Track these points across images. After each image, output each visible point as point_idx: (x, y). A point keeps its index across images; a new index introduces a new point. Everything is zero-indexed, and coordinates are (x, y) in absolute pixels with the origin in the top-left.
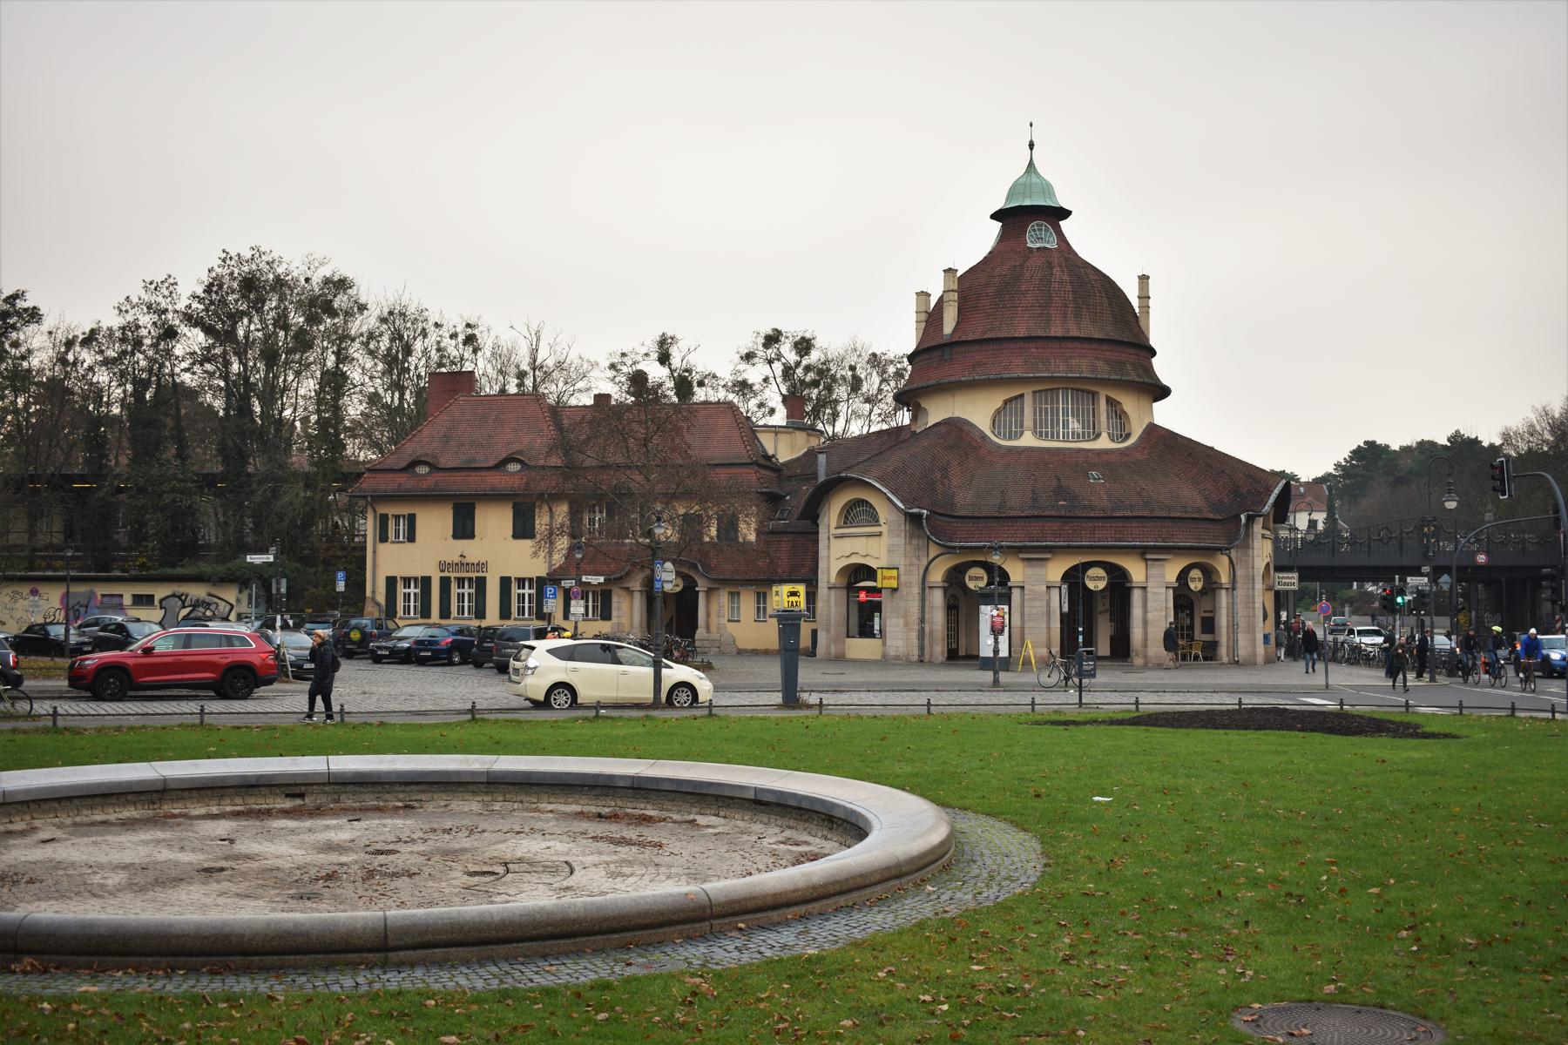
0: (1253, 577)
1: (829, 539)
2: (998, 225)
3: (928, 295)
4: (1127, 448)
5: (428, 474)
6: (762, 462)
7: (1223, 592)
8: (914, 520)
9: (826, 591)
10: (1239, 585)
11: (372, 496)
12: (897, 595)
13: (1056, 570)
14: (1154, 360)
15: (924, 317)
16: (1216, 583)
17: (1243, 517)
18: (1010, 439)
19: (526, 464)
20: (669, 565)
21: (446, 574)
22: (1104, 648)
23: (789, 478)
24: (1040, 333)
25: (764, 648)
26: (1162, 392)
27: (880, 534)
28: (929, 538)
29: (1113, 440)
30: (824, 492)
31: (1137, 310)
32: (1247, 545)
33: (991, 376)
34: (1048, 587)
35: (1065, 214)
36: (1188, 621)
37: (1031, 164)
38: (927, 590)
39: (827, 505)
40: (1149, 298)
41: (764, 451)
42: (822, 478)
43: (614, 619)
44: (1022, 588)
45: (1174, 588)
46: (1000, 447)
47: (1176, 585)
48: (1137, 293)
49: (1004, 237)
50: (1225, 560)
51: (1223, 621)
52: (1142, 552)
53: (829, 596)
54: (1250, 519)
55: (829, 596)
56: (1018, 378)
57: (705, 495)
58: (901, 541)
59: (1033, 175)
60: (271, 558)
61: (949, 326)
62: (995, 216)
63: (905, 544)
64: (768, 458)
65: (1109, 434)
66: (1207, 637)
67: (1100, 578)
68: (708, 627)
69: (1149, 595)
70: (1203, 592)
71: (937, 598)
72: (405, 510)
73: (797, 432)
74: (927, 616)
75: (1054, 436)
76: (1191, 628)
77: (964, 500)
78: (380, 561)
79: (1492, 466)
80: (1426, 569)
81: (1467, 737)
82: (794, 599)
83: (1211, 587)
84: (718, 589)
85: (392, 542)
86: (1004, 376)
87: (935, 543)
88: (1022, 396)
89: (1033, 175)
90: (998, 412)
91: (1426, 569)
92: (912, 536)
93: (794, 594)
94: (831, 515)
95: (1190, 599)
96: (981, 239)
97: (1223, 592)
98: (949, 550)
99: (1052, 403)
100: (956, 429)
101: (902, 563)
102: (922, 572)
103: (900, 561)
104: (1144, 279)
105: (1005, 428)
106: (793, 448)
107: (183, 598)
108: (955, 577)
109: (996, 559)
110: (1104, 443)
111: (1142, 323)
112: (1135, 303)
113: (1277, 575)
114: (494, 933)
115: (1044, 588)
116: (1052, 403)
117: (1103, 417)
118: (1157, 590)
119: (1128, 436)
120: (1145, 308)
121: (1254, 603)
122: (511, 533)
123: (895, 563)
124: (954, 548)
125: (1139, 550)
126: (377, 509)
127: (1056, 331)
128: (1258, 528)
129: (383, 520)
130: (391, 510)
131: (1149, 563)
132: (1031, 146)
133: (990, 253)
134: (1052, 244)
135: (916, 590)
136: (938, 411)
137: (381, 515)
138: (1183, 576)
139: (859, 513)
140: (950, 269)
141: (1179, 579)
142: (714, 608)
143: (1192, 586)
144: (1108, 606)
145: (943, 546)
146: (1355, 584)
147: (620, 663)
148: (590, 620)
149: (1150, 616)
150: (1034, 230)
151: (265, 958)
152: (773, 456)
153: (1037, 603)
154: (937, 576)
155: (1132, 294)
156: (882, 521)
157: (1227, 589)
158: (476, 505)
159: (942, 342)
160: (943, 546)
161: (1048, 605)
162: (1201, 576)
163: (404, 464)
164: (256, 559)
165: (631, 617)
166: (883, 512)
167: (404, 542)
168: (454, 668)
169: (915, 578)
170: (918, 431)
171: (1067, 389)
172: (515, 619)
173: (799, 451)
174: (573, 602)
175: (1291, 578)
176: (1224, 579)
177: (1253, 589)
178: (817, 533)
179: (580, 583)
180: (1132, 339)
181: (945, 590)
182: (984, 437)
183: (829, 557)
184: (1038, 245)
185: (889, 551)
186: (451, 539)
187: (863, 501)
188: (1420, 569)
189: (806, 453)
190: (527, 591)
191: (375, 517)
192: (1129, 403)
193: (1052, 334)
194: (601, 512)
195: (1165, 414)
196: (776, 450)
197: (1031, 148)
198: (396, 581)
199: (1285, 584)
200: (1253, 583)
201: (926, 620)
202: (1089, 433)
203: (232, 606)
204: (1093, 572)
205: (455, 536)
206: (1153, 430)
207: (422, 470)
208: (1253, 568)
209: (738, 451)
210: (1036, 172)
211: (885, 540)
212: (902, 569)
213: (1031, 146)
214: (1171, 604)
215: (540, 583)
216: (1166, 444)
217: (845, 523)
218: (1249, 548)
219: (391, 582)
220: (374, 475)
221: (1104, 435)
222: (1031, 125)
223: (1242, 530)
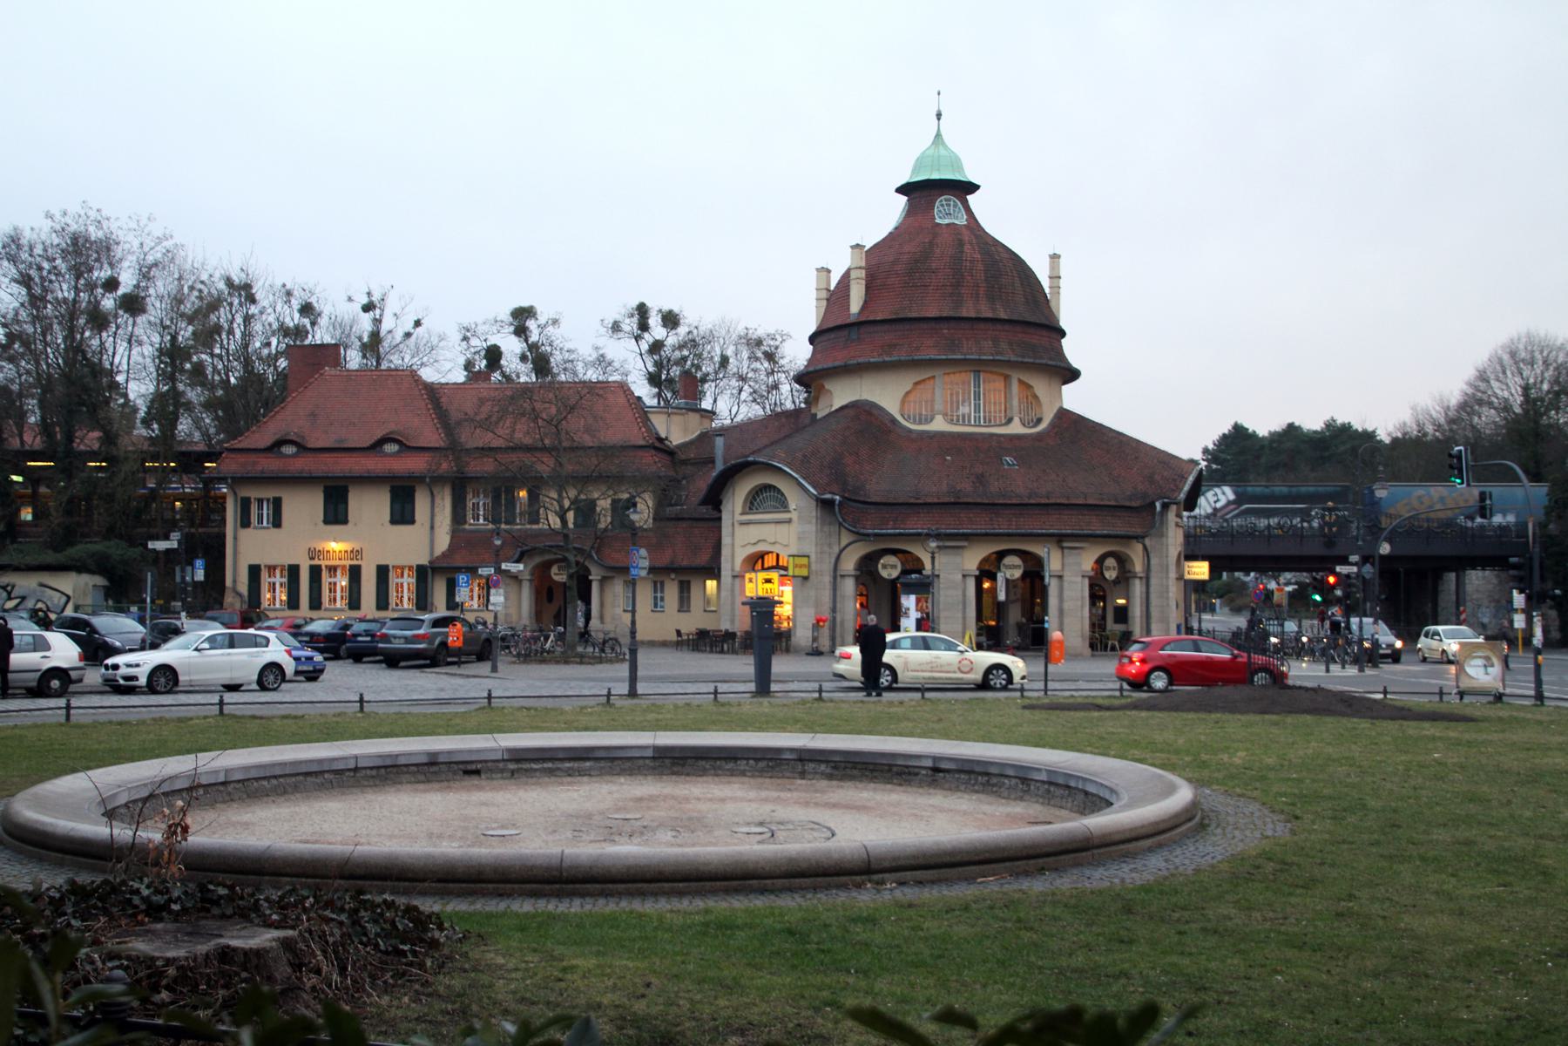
0: (1167, 566)
1: (733, 525)
2: (903, 199)
3: (829, 271)
4: (1038, 434)
5: (294, 456)
6: (657, 444)
7: (1137, 582)
8: (825, 505)
9: (729, 579)
11: (232, 478)
12: (809, 584)
13: (1086, 560)
14: (1063, 341)
15: (824, 294)
16: (1130, 572)
18: (920, 423)
19: (405, 445)
20: (643, 552)
21: (316, 562)
22: (784, 648)
23: (684, 462)
24: (952, 314)
25: (661, 639)
26: (1072, 375)
27: (789, 521)
28: (840, 524)
29: (1024, 425)
30: (733, 473)
31: (1047, 290)
32: (1162, 535)
33: (903, 358)
34: (964, 576)
35: (972, 188)
37: (938, 135)
38: (839, 578)
39: (731, 490)
40: (1060, 277)
41: (657, 434)
42: (720, 466)
45: (1090, 578)
46: (910, 431)
47: (977, 573)
48: (1047, 273)
49: (911, 211)
50: (1139, 547)
51: (1137, 612)
52: (1059, 539)
53: (733, 585)
54: (1165, 506)
55: (733, 585)
56: (930, 360)
57: (613, 480)
58: (812, 528)
59: (941, 147)
60: (175, 545)
61: (855, 305)
62: (901, 190)
63: (817, 532)
64: (661, 440)
66: (1120, 628)
67: (1015, 567)
68: (602, 618)
69: (1066, 585)
70: (1116, 582)
71: (849, 586)
72: (270, 493)
73: (690, 413)
74: (838, 605)
77: (878, 486)
78: (242, 548)
79: (1450, 456)
80: (1354, 558)
82: (768, 586)
83: (1125, 577)
84: (613, 578)
85: (255, 528)
86: (916, 358)
87: (846, 528)
88: (934, 377)
89: (941, 147)
90: (908, 393)
91: (1354, 558)
92: (823, 524)
93: (768, 581)
94: (736, 497)
96: (889, 213)
97: (1137, 582)
98: (862, 537)
100: (863, 413)
101: (813, 549)
102: (833, 560)
103: (810, 549)
104: (1055, 257)
106: (686, 430)
107: (9, 588)
108: (867, 569)
109: (1039, 550)
110: (1016, 428)
111: (1053, 305)
114: (948, 858)
117: (1015, 402)
118: (1073, 579)
119: (1039, 421)
120: (1056, 288)
121: (1168, 592)
122: (388, 517)
123: (806, 551)
124: (868, 535)
125: (1055, 539)
126: (238, 491)
127: (968, 311)
128: (1171, 516)
129: (245, 505)
130: (253, 493)
131: (1066, 551)
132: (939, 116)
133: (896, 228)
134: (961, 220)
135: (827, 579)
136: (841, 394)
137: (242, 499)
139: (765, 499)
140: (858, 245)
142: (609, 598)
145: (857, 533)
146: (1225, 574)
149: (1066, 606)
150: (942, 205)
151: (775, 881)
152: (667, 439)
154: (849, 564)
156: (792, 506)
157: (1141, 578)
158: (417, 488)
159: (848, 321)
160: (857, 533)
161: (964, 595)
162: (1116, 565)
163: (269, 443)
164: (160, 545)
165: (520, 607)
166: (794, 499)
167: (268, 528)
168: (341, 662)
169: (827, 566)
170: (819, 416)
171: (979, 371)
172: (393, 610)
173: (693, 433)
176: (1138, 567)
178: (720, 519)
179: (499, 570)
180: (1043, 321)
181: (857, 578)
182: (894, 421)
183: (733, 545)
184: (946, 221)
185: (799, 538)
186: (388, 524)
187: (775, 487)
188: (1347, 558)
189: (699, 435)
191: (236, 501)
192: (1040, 386)
193: (965, 314)
194: (219, 489)
195: (1074, 398)
196: (668, 432)
197: (939, 119)
198: (321, 570)
200: (1167, 572)
201: (838, 609)
202: (1000, 417)
203: (69, 598)
204: (1009, 560)
205: (394, 521)
206: (1064, 416)
207: (289, 450)
208: (1167, 557)
209: (637, 437)
210: (943, 143)
211: (795, 528)
213: (939, 116)
216: (1071, 424)
217: (750, 509)
219: (255, 571)
220: (233, 456)
221: (1016, 420)
222: (939, 94)
223: (1157, 518)
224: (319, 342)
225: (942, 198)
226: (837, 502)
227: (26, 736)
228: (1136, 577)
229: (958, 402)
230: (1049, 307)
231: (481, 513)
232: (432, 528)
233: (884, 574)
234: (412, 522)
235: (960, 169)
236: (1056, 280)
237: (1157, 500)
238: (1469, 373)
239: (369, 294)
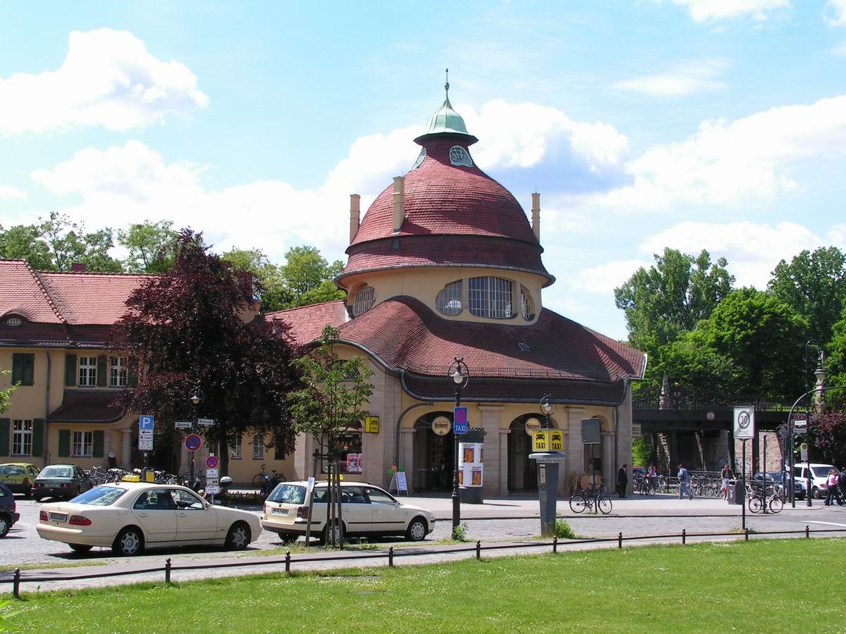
16: (604, 431)
25: (239, 482)
26: (550, 280)
31: (530, 220)
35: (473, 140)
65: (470, 311)
75: (483, 315)
81: (111, 429)
111: (535, 231)
132: (447, 86)
147: (414, 541)
148: (82, 457)
150: (454, 152)
154: (410, 422)
190: (23, 432)
195: (551, 299)
197: (447, 90)
212: (382, 417)
213: (447, 86)
215: (39, 425)
222: (447, 71)
227: (731, 501)
229: (505, 303)
231: (118, 377)
232: (48, 388)
233: (437, 431)
234: (31, 383)
235: (464, 128)
238: (250, 249)
239: (656, 256)
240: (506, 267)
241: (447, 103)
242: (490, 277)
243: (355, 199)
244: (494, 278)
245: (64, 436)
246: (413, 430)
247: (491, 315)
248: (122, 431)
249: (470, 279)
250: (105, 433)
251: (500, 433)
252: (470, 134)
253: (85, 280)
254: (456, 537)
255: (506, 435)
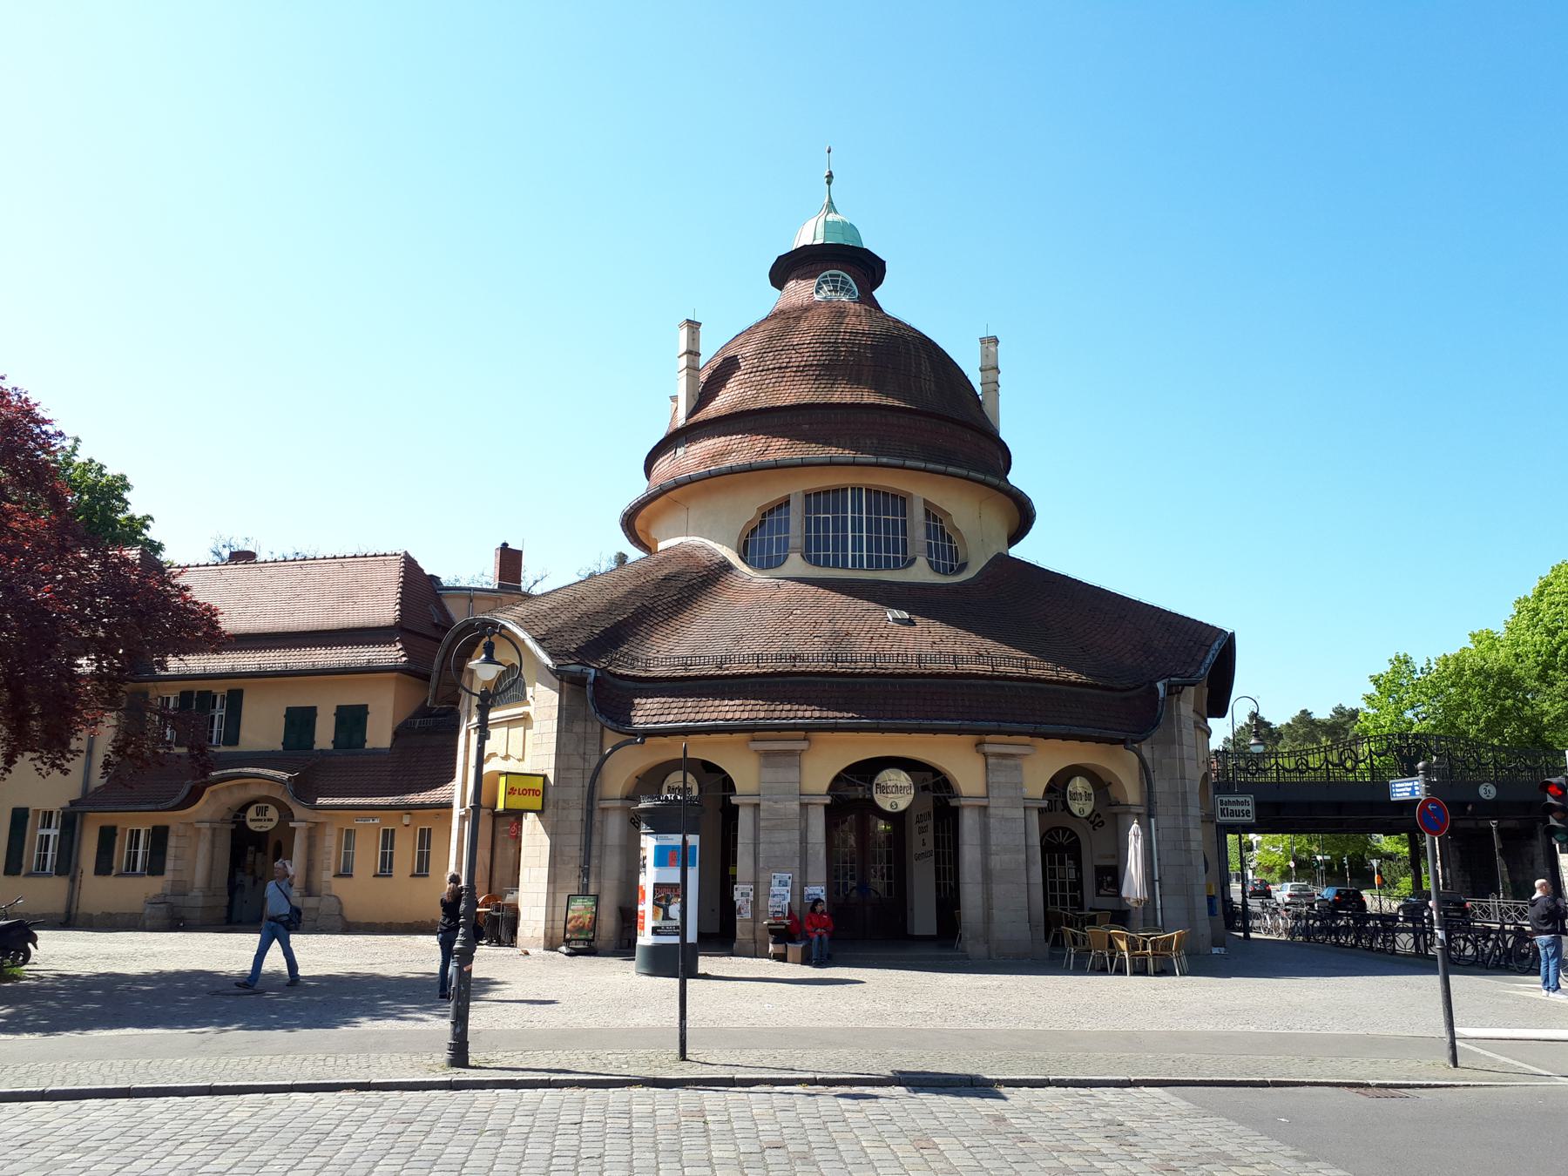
0: (1184, 794)
10: (1159, 809)
16: (1118, 804)
17: (1160, 685)
31: (979, 390)
34: (804, 806)
36: (1072, 874)
43: (169, 875)
44: (757, 806)
45: (1041, 811)
65: (930, 563)
67: (899, 789)
70: (1095, 820)
76: (1078, 885)
95: (1073, 833)
99: (835, 511)
105: (761, 552)
111: (987, 408)
112: (975, 379)
113: (1219, 798)
115: (795, 806)
116: (835, 511)
119: (963, 567)
120: (992, 385)
121: (1188, 841)
138: (1057, 787)
141: (1050, 789)
143: (1075, 807)
144: (930, 846)
149: (995, 862)
153: (782, 836)
155: (971, 367)
161: (804, 840)
162: (1090, 791)
174: (680, 844)
175: (1242, 803)
177: (1185, 815)
188: (260, 852)
197: (829, 183)
199: (1233, 813)
200: (1185, 806)
208: (1183, 778)
213: (830, 176)
214: (1036, 839)
218: (1173, 742)
224: (236, 550)
225: (827, 273)
226: (591, 679)
228: (1128, 813)
230: (983, 412)
236: (991, 374)
237: (1160, 678)
240: (941, 468)
241: (831, 207)
242: (853, 489)
243: (693, 326)
244: (860, 489)
245: (107, 837)
246: (828, 800)
247: (854, 564)
248: (197, 825)
249: (808, 496)
250: (171, 829)
251: (987, 797)
252: (865, 247)
253: (263, 570)
254: (459, 1055)
255: (823, 808)
